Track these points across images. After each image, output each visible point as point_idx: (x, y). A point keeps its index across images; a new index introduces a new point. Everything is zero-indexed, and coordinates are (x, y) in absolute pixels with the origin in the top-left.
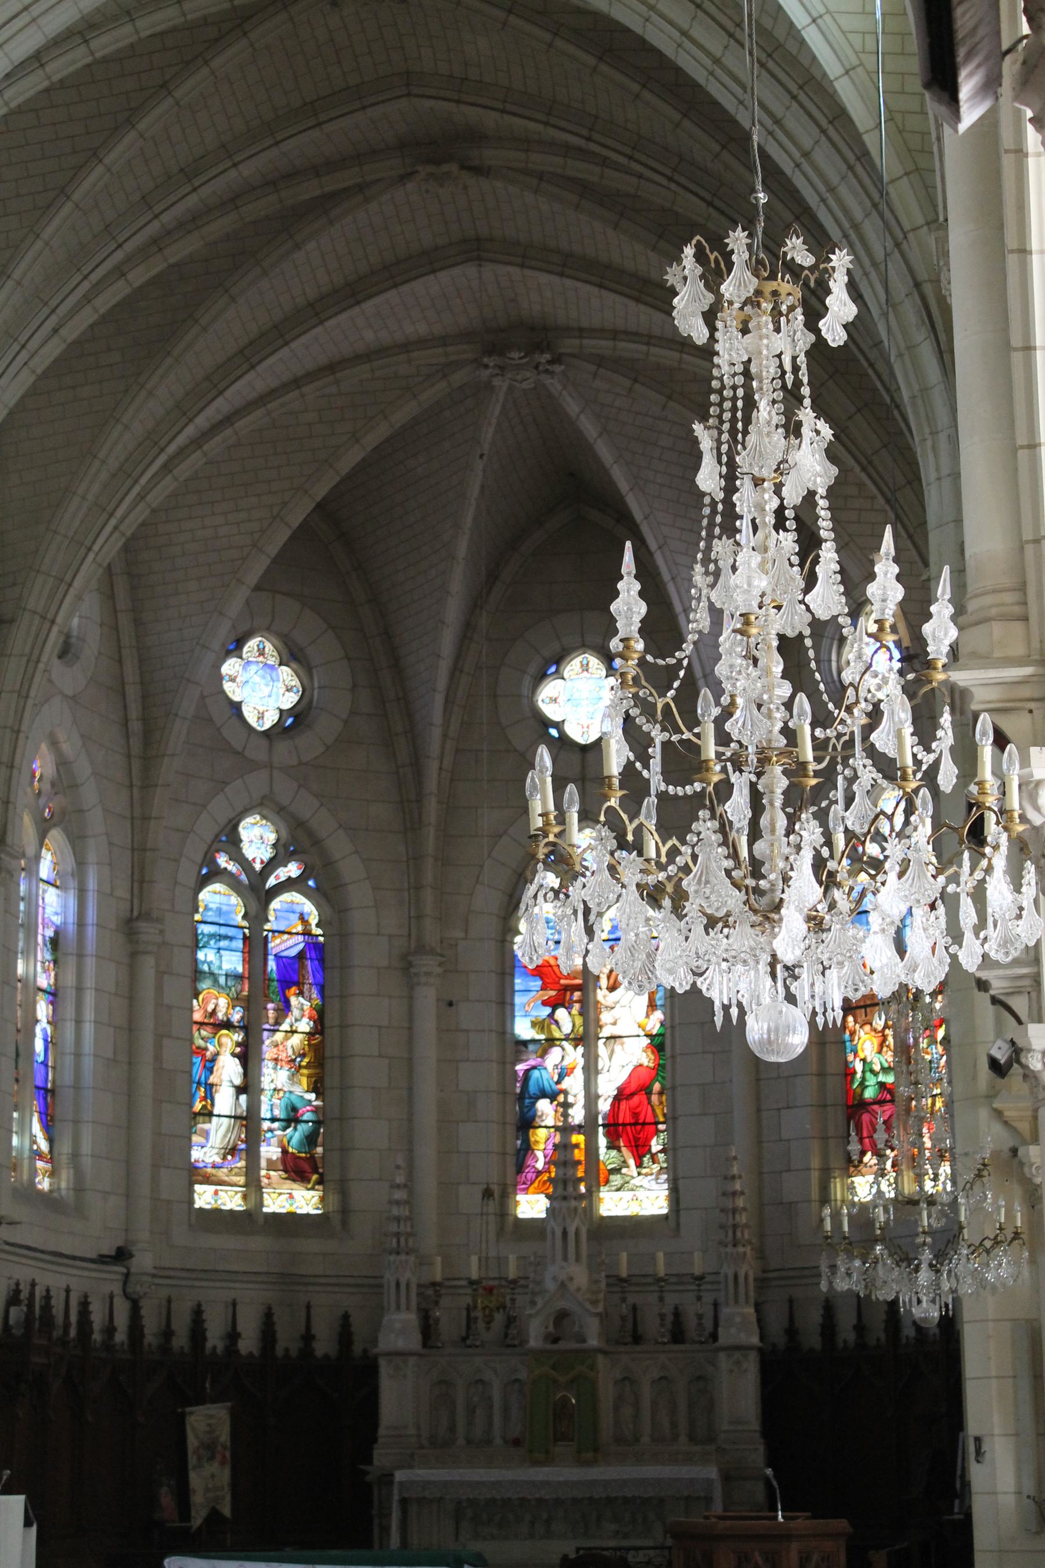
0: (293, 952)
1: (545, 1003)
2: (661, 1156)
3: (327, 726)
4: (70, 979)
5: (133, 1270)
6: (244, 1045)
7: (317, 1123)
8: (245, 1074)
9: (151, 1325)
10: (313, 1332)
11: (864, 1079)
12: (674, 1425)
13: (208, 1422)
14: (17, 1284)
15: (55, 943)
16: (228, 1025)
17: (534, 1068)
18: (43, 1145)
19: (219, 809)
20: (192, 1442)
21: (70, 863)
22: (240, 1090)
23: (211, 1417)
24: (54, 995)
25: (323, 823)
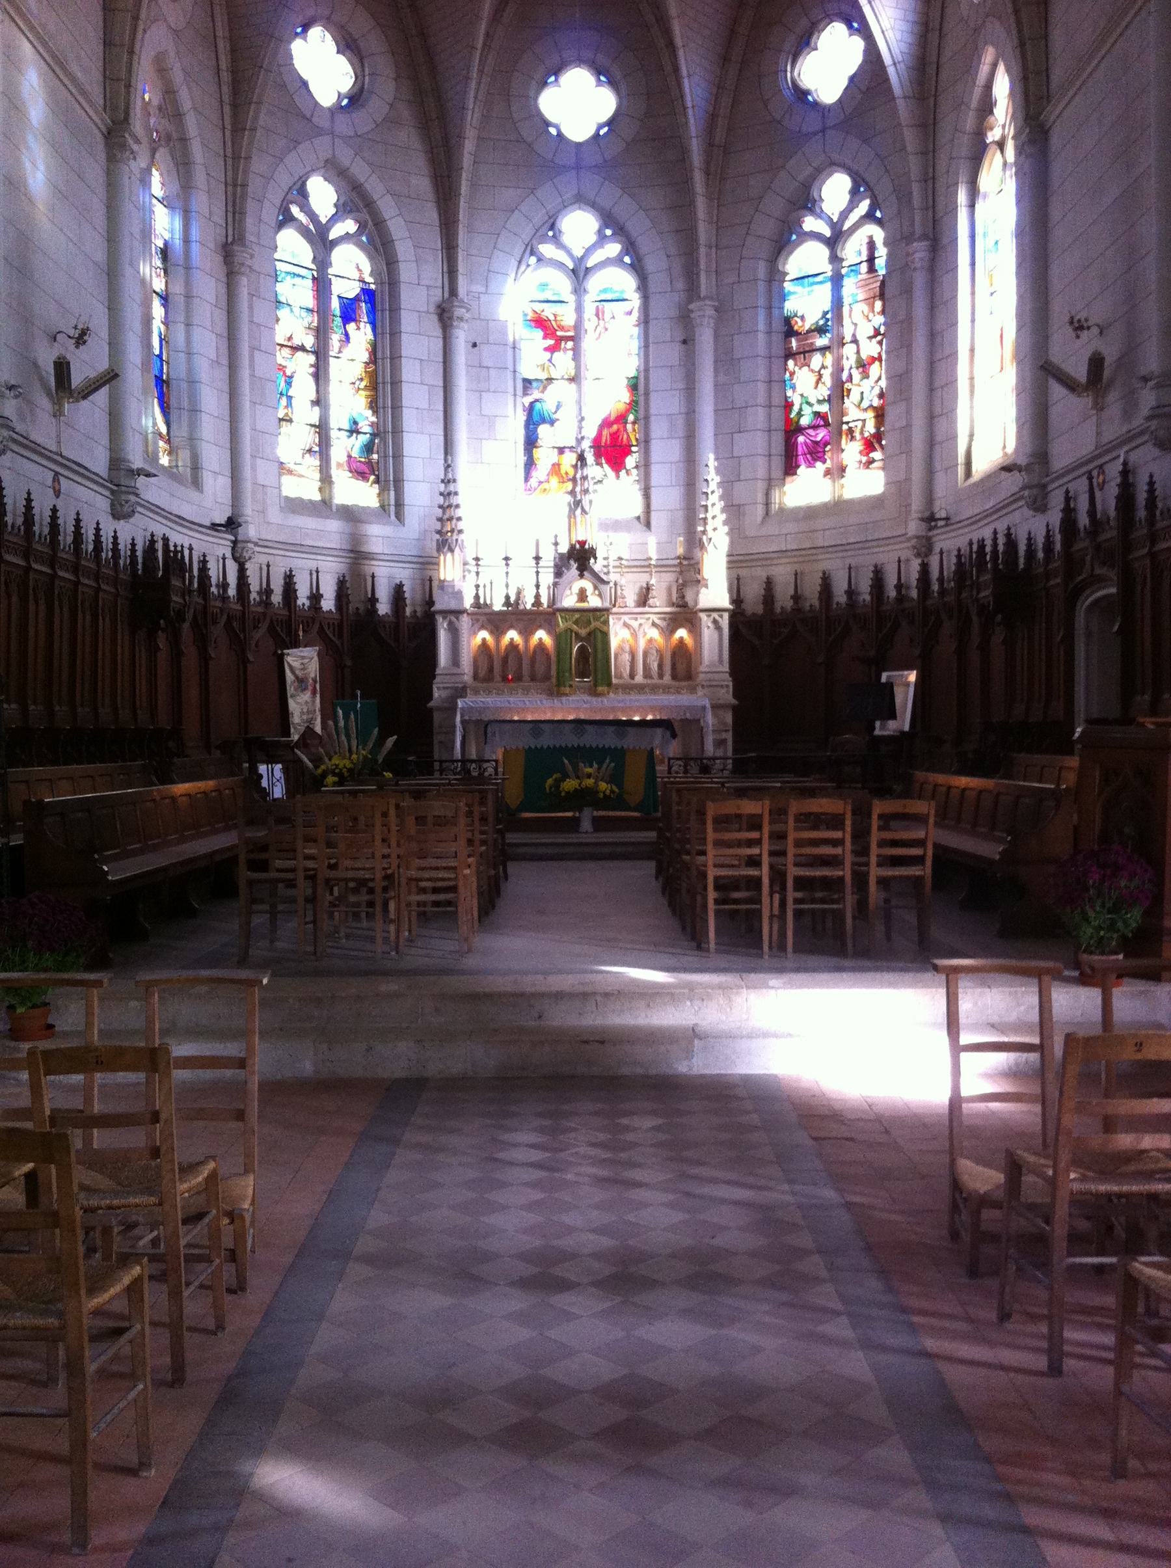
0: (351, 295)
1: (546, 349)
2: (635, 472)
3: (377, 107)
4: (178, 288)
5: (239, 538)
6: (317, 366)
7: (374, 435)
8: (318, 391)
9: (254, 585)
10: (377, 596)
11: (801, 409)
12: (660, 666)
13: (303, 661)
14: (152, 535)
15: (165, 253)
16: (302, 348)
17: (537, 401)
18: (163, 429)
19: (284, 180)
20: (289, 676)
21: (175, 187)
22: (317, 402)
23: (303, 658)
24: (165, 299)
25: (375, 187)
